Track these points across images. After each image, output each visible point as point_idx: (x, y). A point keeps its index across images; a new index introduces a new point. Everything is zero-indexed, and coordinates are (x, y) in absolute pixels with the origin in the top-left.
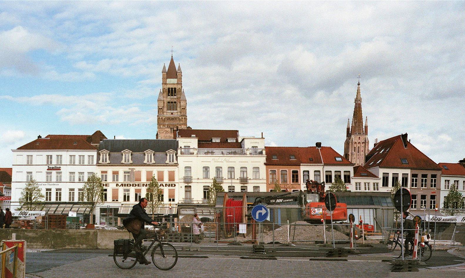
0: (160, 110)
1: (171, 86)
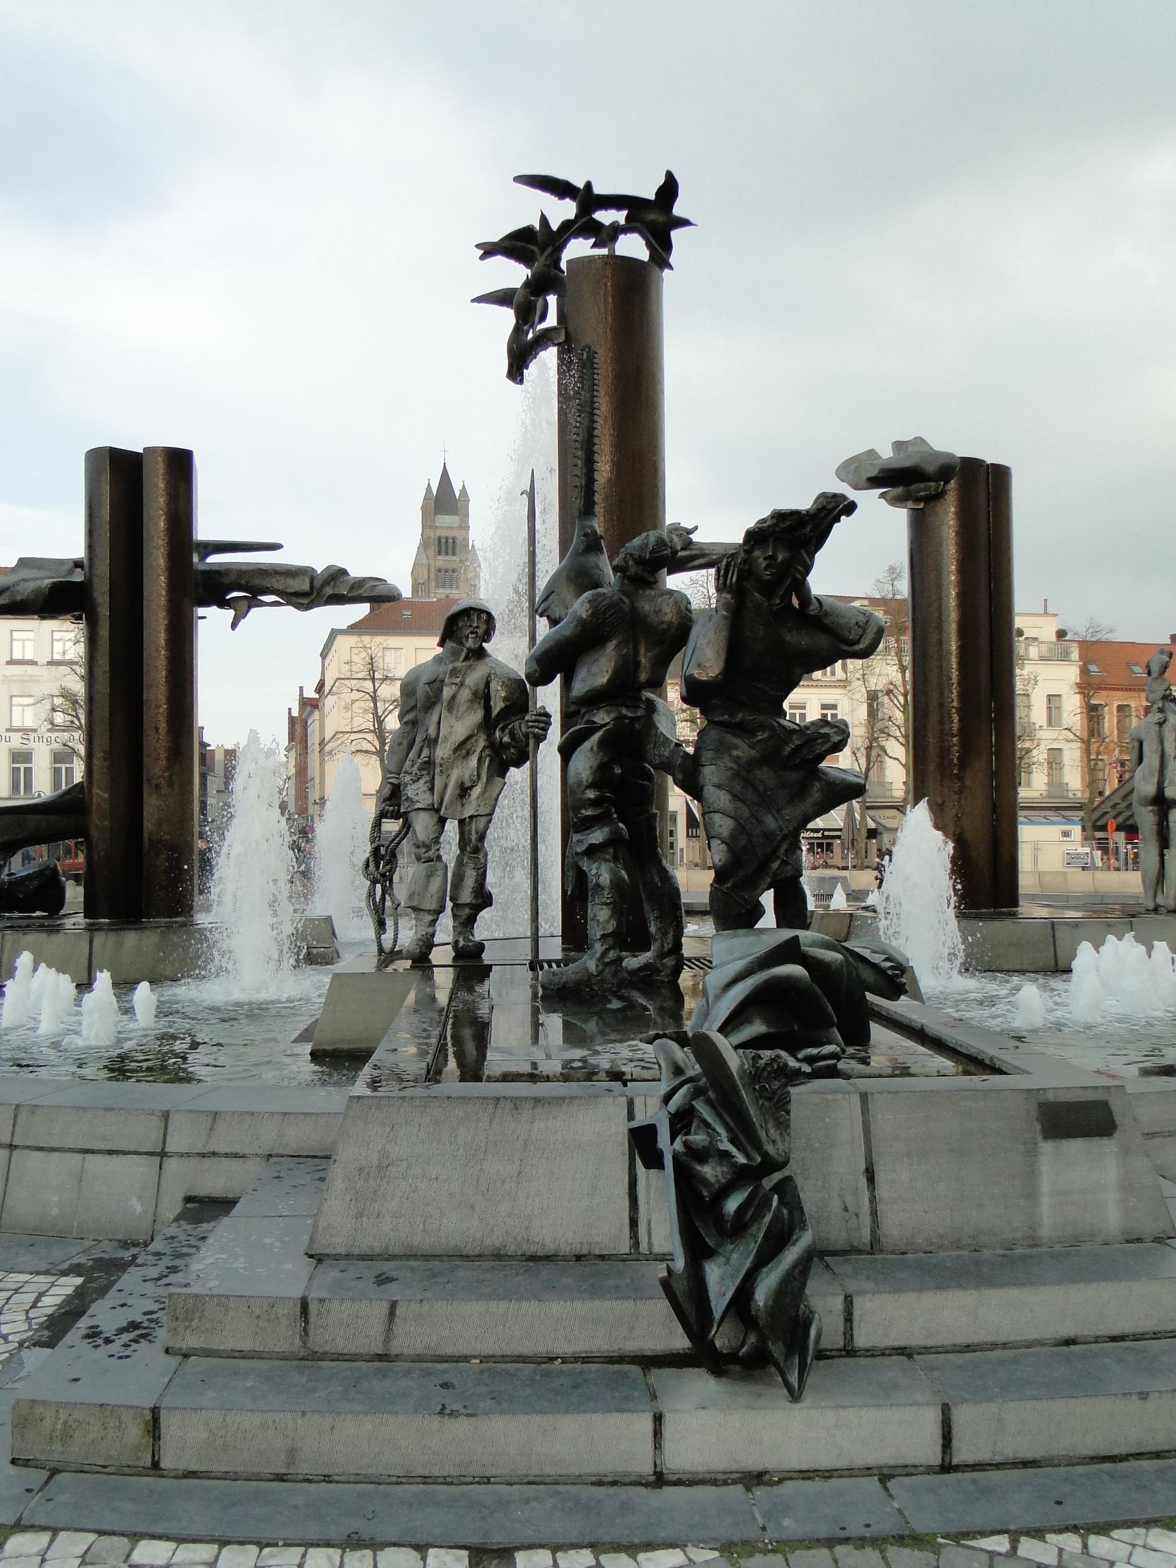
1: (443, 533)
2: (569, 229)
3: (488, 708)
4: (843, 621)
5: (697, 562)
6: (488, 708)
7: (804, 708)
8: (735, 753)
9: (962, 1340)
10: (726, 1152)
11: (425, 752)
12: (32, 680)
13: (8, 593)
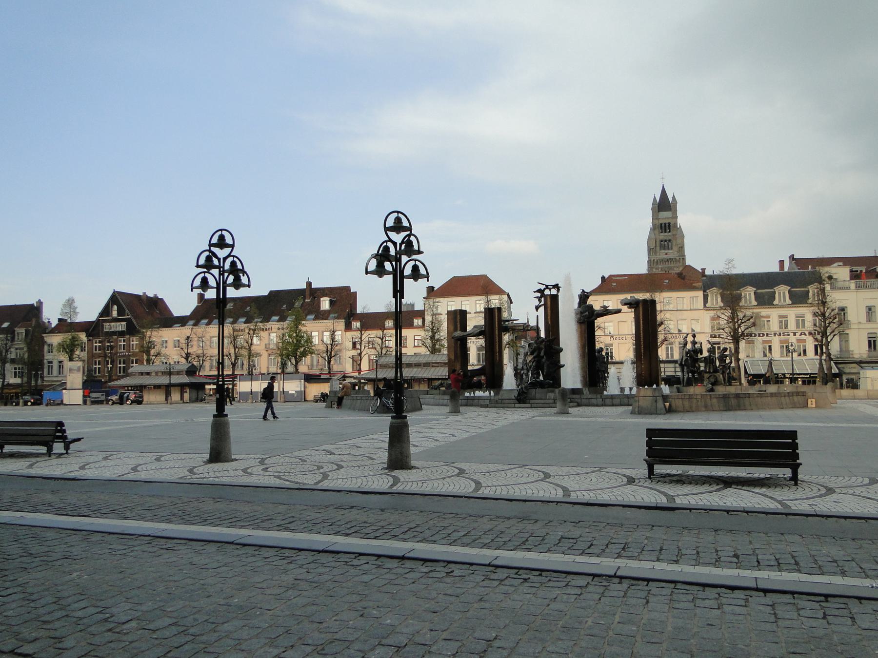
0: (650, 250)
1: (663, 221)
2: (545, 289)
7: (804, 317)
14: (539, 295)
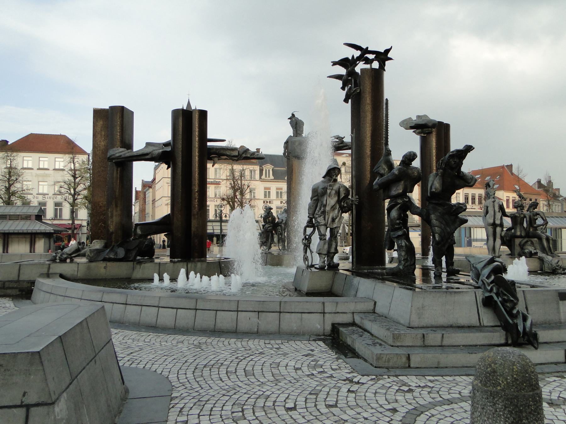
3: (339, 196)
4: (468, 177)
5: (345, 148)
6: (339, 196)
8: (439, 211)
9: (557, 341)
10: (512, 300)
11: (322, 209)
12: (47, 176)
13: (150, 155)
14: (342, 71)
